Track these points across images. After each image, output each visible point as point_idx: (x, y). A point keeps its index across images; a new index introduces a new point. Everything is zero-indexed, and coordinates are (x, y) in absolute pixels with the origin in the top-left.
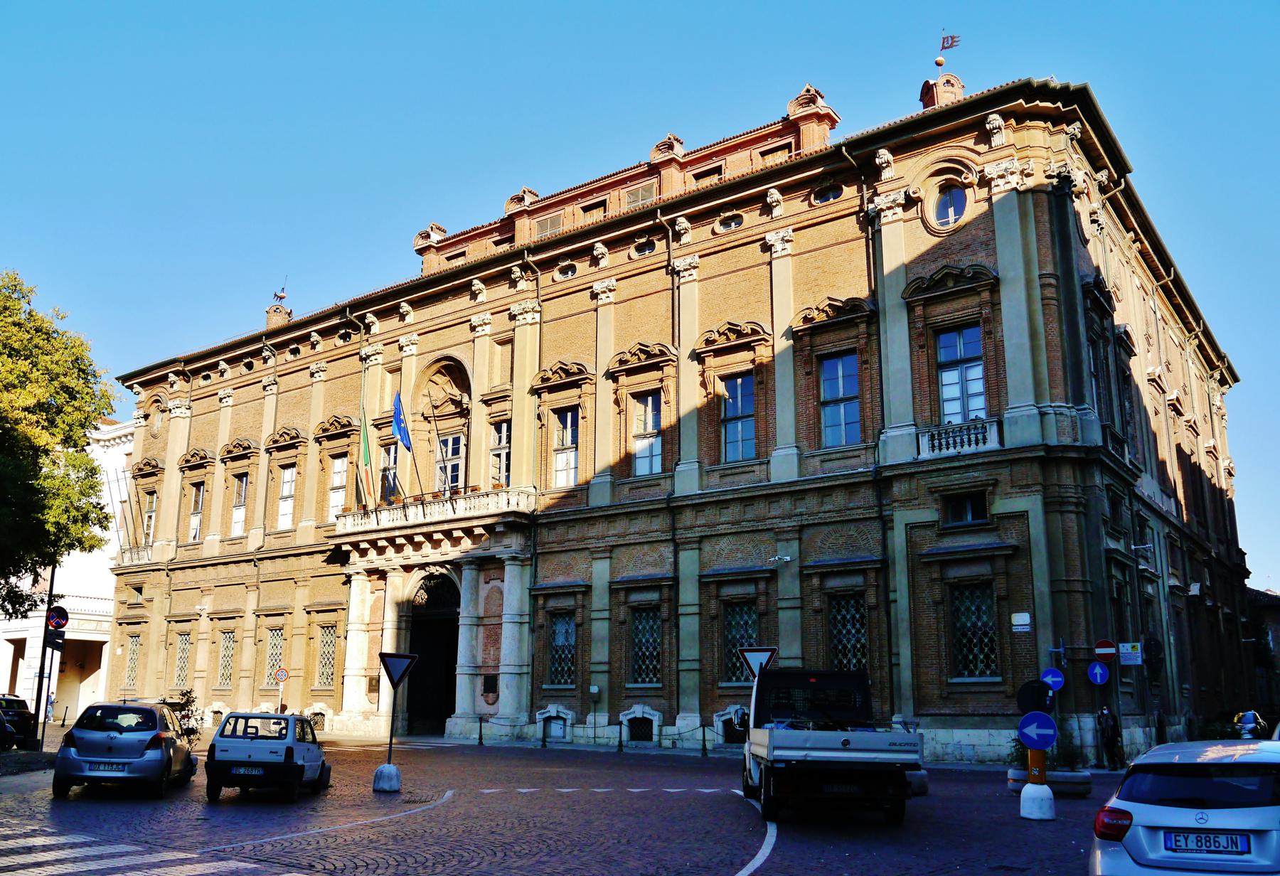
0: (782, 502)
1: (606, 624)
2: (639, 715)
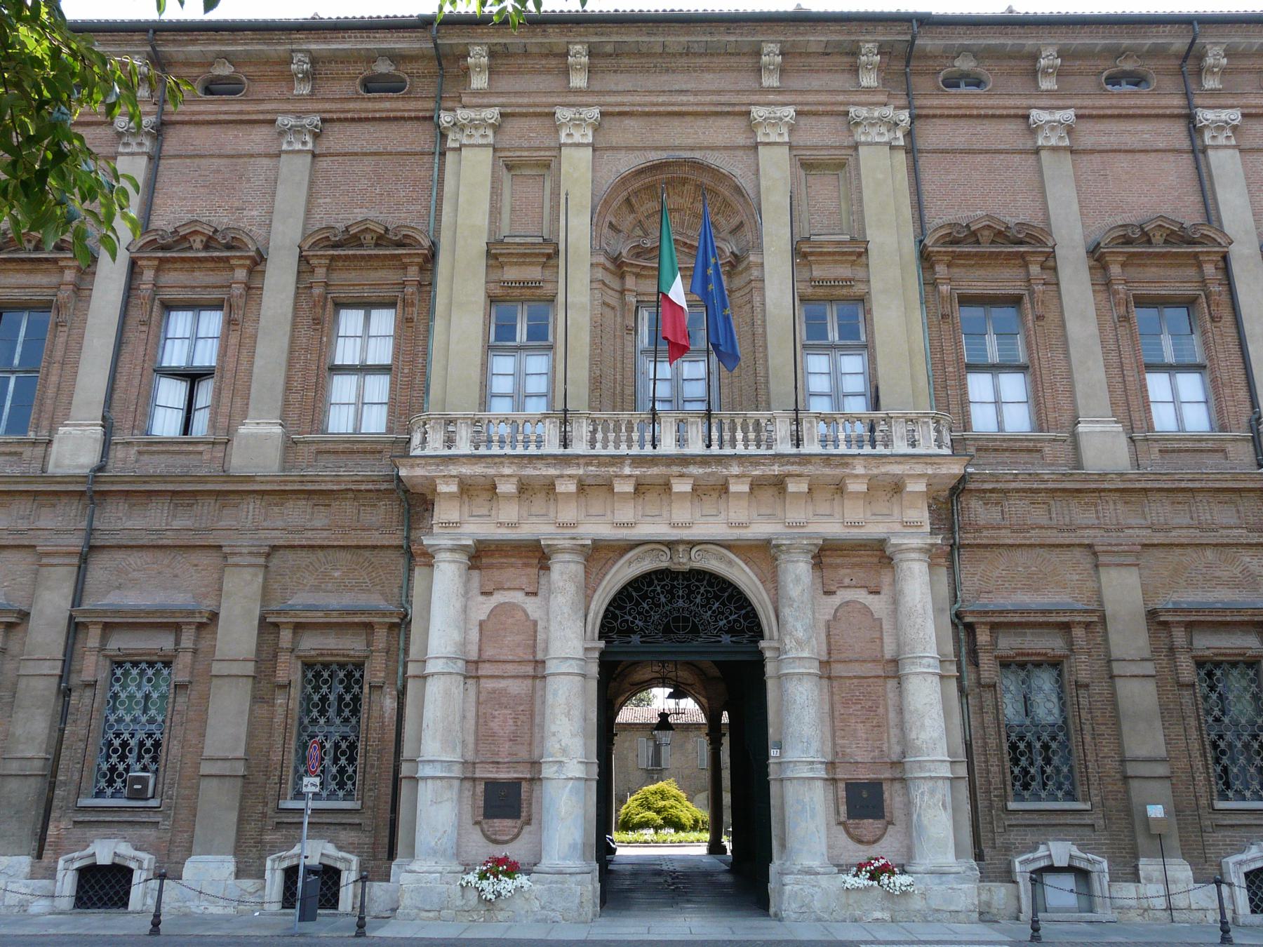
0: (197, 509)
1: (1151, 686)
2: (104, 858)
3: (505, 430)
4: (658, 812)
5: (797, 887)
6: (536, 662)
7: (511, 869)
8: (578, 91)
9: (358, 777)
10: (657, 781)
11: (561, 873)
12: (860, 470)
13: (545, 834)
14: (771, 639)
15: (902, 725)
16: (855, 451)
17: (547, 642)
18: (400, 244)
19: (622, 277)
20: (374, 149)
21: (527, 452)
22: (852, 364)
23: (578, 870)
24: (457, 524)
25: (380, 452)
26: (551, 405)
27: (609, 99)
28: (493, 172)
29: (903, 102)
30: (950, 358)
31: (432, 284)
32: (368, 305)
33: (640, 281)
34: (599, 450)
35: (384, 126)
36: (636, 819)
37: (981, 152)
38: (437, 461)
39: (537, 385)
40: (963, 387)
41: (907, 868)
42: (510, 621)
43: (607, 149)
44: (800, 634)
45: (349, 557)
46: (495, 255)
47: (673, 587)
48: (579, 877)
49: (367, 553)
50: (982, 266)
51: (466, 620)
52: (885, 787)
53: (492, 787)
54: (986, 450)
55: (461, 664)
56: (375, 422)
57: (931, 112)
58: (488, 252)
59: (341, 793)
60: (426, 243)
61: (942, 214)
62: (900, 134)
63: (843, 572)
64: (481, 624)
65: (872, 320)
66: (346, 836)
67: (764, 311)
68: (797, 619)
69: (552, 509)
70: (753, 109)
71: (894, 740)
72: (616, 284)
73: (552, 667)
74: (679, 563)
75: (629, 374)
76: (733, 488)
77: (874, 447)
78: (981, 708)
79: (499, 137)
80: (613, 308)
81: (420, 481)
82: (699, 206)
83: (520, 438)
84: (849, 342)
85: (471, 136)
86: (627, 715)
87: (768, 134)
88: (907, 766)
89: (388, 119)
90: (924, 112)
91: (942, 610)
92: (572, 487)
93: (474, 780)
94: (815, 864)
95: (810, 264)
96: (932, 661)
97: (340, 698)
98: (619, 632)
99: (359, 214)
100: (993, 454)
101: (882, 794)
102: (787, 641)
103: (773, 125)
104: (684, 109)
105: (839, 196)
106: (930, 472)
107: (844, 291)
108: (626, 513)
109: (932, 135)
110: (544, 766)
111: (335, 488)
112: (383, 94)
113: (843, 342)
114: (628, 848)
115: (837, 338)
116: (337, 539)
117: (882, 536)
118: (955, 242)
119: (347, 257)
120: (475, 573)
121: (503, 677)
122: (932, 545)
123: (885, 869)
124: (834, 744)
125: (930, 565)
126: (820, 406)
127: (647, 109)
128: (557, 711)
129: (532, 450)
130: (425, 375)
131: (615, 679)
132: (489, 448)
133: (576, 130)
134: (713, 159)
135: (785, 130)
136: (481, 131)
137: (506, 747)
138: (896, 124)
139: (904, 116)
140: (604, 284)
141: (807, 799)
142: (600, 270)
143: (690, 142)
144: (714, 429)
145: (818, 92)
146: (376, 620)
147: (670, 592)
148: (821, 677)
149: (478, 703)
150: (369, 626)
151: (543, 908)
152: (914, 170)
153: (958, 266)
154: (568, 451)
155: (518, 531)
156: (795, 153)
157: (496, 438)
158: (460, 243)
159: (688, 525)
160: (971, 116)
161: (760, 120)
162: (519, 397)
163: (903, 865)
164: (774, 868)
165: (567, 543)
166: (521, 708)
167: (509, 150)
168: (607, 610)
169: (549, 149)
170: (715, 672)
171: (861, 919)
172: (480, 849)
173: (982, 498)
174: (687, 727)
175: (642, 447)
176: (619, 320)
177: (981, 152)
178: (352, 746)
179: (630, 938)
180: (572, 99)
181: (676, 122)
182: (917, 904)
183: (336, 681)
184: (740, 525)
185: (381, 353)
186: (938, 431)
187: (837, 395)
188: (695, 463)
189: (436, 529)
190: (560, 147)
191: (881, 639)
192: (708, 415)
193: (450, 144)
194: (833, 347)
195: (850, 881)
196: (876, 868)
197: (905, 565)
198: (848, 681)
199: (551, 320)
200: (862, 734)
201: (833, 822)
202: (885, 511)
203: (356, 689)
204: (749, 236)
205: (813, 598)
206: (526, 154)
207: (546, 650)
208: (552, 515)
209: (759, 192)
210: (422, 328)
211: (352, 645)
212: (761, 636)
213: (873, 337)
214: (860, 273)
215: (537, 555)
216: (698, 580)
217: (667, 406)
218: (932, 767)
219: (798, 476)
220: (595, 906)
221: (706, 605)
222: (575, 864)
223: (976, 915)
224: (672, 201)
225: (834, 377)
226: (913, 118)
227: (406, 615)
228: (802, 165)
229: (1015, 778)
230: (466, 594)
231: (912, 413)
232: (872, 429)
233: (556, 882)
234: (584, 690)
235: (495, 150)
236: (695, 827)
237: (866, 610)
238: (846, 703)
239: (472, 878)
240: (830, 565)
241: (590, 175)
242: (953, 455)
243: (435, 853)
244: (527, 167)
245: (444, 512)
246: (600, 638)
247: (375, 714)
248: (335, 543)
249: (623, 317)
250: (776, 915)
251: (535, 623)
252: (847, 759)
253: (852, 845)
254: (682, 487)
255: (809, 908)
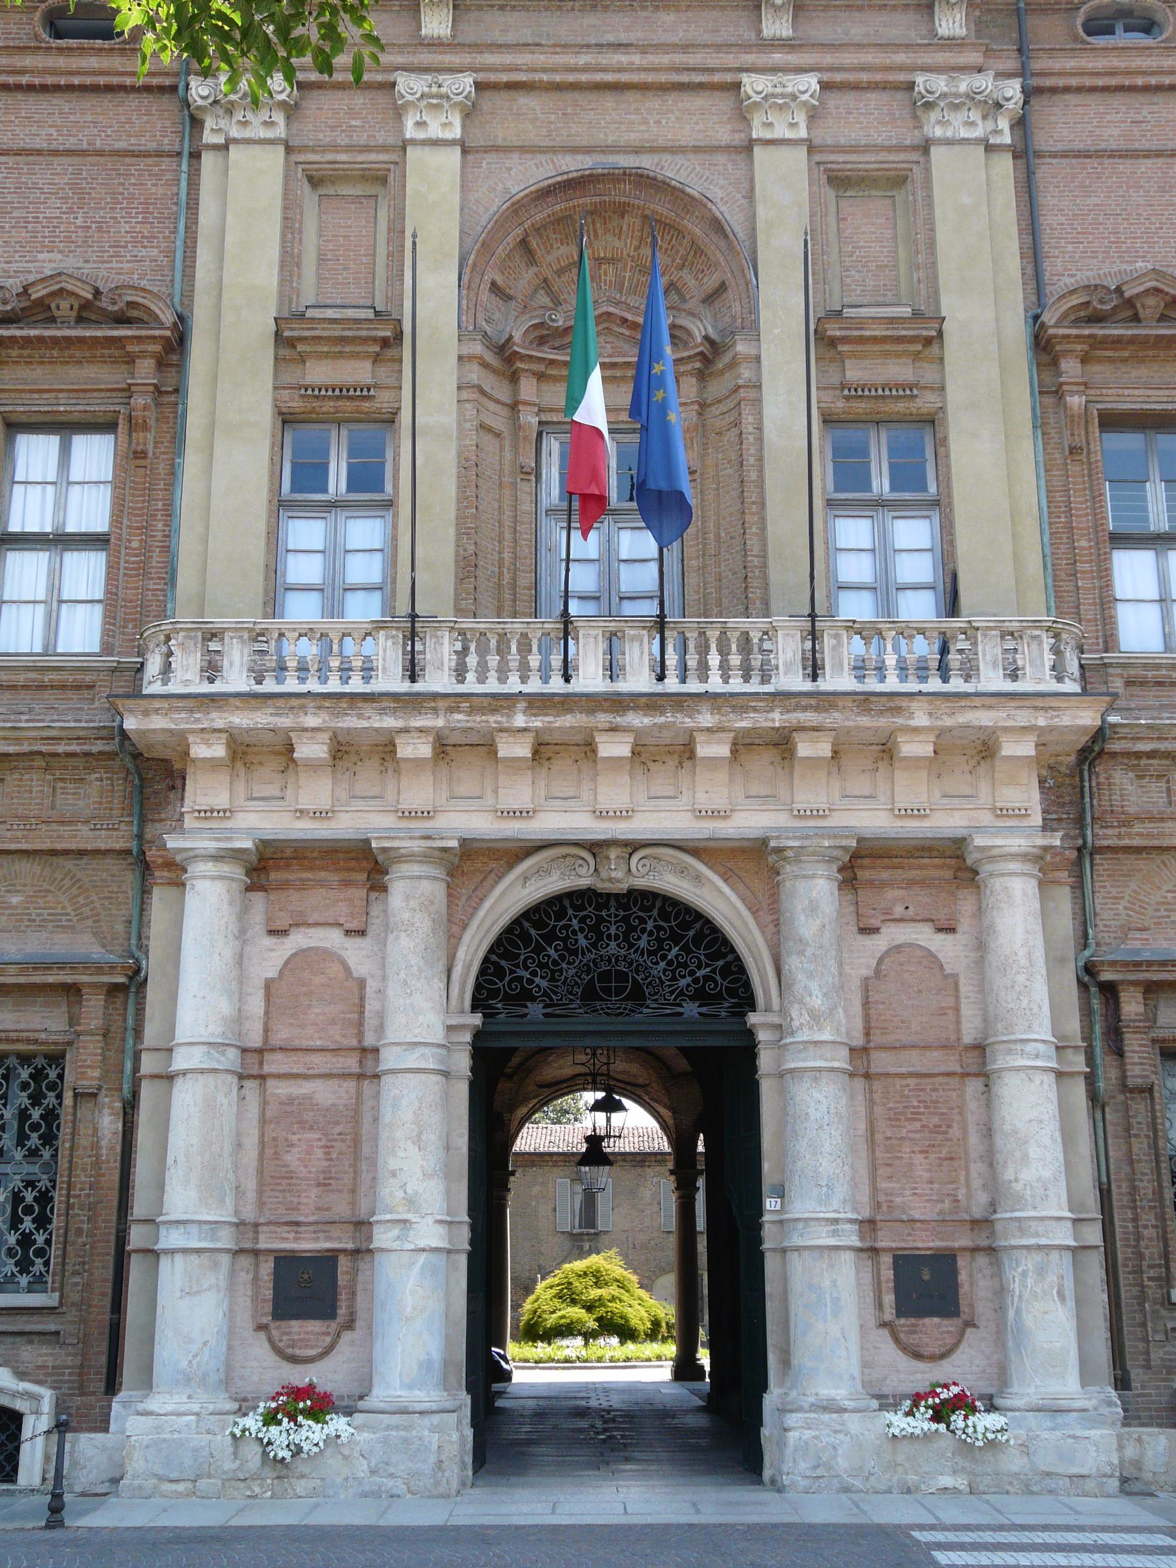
3: (308, 649)
4: (589, 1307)
5: (808, 1434)
6: (364, 1050)
7: (319, 1405)
8: (436, 44)
9: (54, 1252)
10: (590, 1253)
11: (404, 1412)
12: (921, 719)
13: (377, 1346)
14: (768, 1009)
15: (990, 1157)
16: (912, 686)
17: (381, 1015)
18: (121, 319)
19: (514, 378)
20: (71, 143)
21: (347, 689)
22: (913, 533)
23: (434, 1406)
24: (226, 813)
25: (91, 687)
26: (389, 605)
27: (490, 59)
28: (285, 197)
29: (1011, 64)
30: (1083, 522)
31: (179, 390)
32: (64, 427)
33: (545, 387)
34: (471, 685)
35: (89, 102)
36: (551, 1320)
37: (1148, 154)
38: (190, 703)
39: (365, 569)
40: (1104, 574)
41: (998, 1402)
42: (318, 980)
43: (487, 150)
44: (817, 1001)
45: (37, 869)
46: (290, 339)
47: (600, 919)
48: (436, 1419)
49: (69, 864)
50: (1141, 361)
51: (242, 980)
52: (961, 1262)
53: (288, 1266)
54: (1142, 684)
55: (233, 1054)
56: (81, 634)
57: (1061, 82)
58: (278, 334)
59: (24, 1280)
60: (168, 318)
61: (1075, 268)
62: (1004, 124)
63: (891, 894)
64: (268, 985)
65: (947, 456)
66: (30, 1354)
67: (760, 439)
68: (811, 975)
69: (391, 786)
70: (746, 79)
71: (976, 1183)
72: (502, 391)
73: (390, 1059)
74: (610, 880)
75: (526, 551)
76: (704, 750)
77: (945, 679)
78: (1128, 1129)
79: (295, 126)
80: (498, 435)
81: (160, 738)
82: (646, 251)
83: (335, 663)
84: (907, 496)
85: (245, 124)
86: (534, 1137)
87: (771, 125)
88: (999, 1227)
89: (95, 89)
90: (1048, 82)
91: (1062, 960)
92: (425, 750)
93: (256, 1253)
94: (839, 1393)
95: (841, 359)
96: (1041, 1047)
97: (23, 1115)
98: (507, 998)
99: (48, 263)
100: (1155, 691)
101: (954, 1272)
102: (794, 1013)
103: (781, 107)
104: (624, 78)
105: (895, 237)
106: (1041, 722)
107: (900, 406)
108: (519, 792)
109: (1063, 124)
110: (377, 1229)
111: (11, 749)
112: (85, 42)
113: (896, 496)
114: (531, 1371)
115: (886, 487)
116: (14, 839)
117: (959, 833)
118: (1097, 318)
119: (28, 341)
120: (258, 898)
121: (306, 1077)
122: (1046, 849)
123: (960, 1403)
124: (874, 1189)
125: (1042, 884)
126: (857, 607)
127: (558, 78)
128: (399, 1134)
129: (356, 685)
130: (169, 551)
131: (510, 1077)
132: (280, 680)
133: (431, 120)
134: (673, 170)
135: (801, 118)
136: (264, 115)
137: (311, 1197)
138: (998, 105)
139: (1013, 89)
140: (483, 392)
141: (826, 1283)
142: (475, 367)
143: (633, 138)
144: (670, 649)
145: (859, 46)
146: (85, 979)
147: (595, 929)
148: (852, 1075)
149: (263, 1121)
150: (72, 991)
151: (373, 1472)
152: (1028, 190)
153: (1100, 360)
154: (419, 687)
155: (333, 824)
156: (817, 158)
157: (292, 664)
158: (228, 318)
159: (625, 814)
160: (1132, 89)
161: (757, 98)
162: (333, 592)
163: (991, 1397)
164: (770, 1401)
165: (417, 846)
166: (338, 1129)
167: (313, 150)
168: (486, 960)
169: (383, 149)
170: (683, 1064)
171: (918, 1489)
172: (267, 1372)
173: (1133, 768)
174: (640, 1159)
175: (546, 679)
176: (508, 455)
177: (1148, 154)
178: (44, 1198)
179: (522, 1521)
180: (426, 58)
181: (609, 101)
182: (1013, 1462)
183: (15, 1086)
184: (715, 814)
185: (91, 511)
186: (1056, 651)
187: (885, 589)
188: (636, 708)
189: (189, 822)
190: (404, 146)
191: (957, 1009)
192: (661, 624)
193: (209, 137)
194: (880, 504)
195: (899, 1422)
196: (944, 1402)
197: (997, 884)
198: (899, 1082)
199: (389, 455)
200: (921, 1172)
201: (872, 1322)
202: (968, 791)
203: (51, 1099)
204: (736, 308)
205: (840, 939)
206: (343, 157)
207: (381, 1028)
208: (390, 795)
209: (754, 229)
210: (162, 468)
211: (42, 1023)
212: (750, 1003)
213: (949, 486)
214: (929, 375)
215: (365, 866)
216: (643, 909)
217: (590, 608)
218: (1041, 1229)
219: (815, 729)
220: (463, 1467)
221: (658, 951)
222: (428, 1396)
223: (1114, 1483)
224: (606, 243)
225: (878, 556)
226: (1029, 93)
227: (138, 971)
228: (830, 180)
229: (40, 1253)
230: (242, 933)
231: (1013, 620)
232: (944, 650)
233: (397, 1428)
234: (446, 1096)
235: (289, 150)
236: (653, 1334)
237: (932, 960)
238: (895, 1119)
239: (252, 1422)
240: (871, 883)
241: (456, 198)
242: (1085, 692)
243: (188, 1380)
244: (347, 183)
245: (203, 792)
246: (474, 1008)
247: (84, 1141)
248: (13, 847)
249: (515, 448)
250: (773, 1482)
251: (362, 984)
252: (897, 1214)
253: (904, 1362)
254: (614, 748)
255: (829, 1468)
